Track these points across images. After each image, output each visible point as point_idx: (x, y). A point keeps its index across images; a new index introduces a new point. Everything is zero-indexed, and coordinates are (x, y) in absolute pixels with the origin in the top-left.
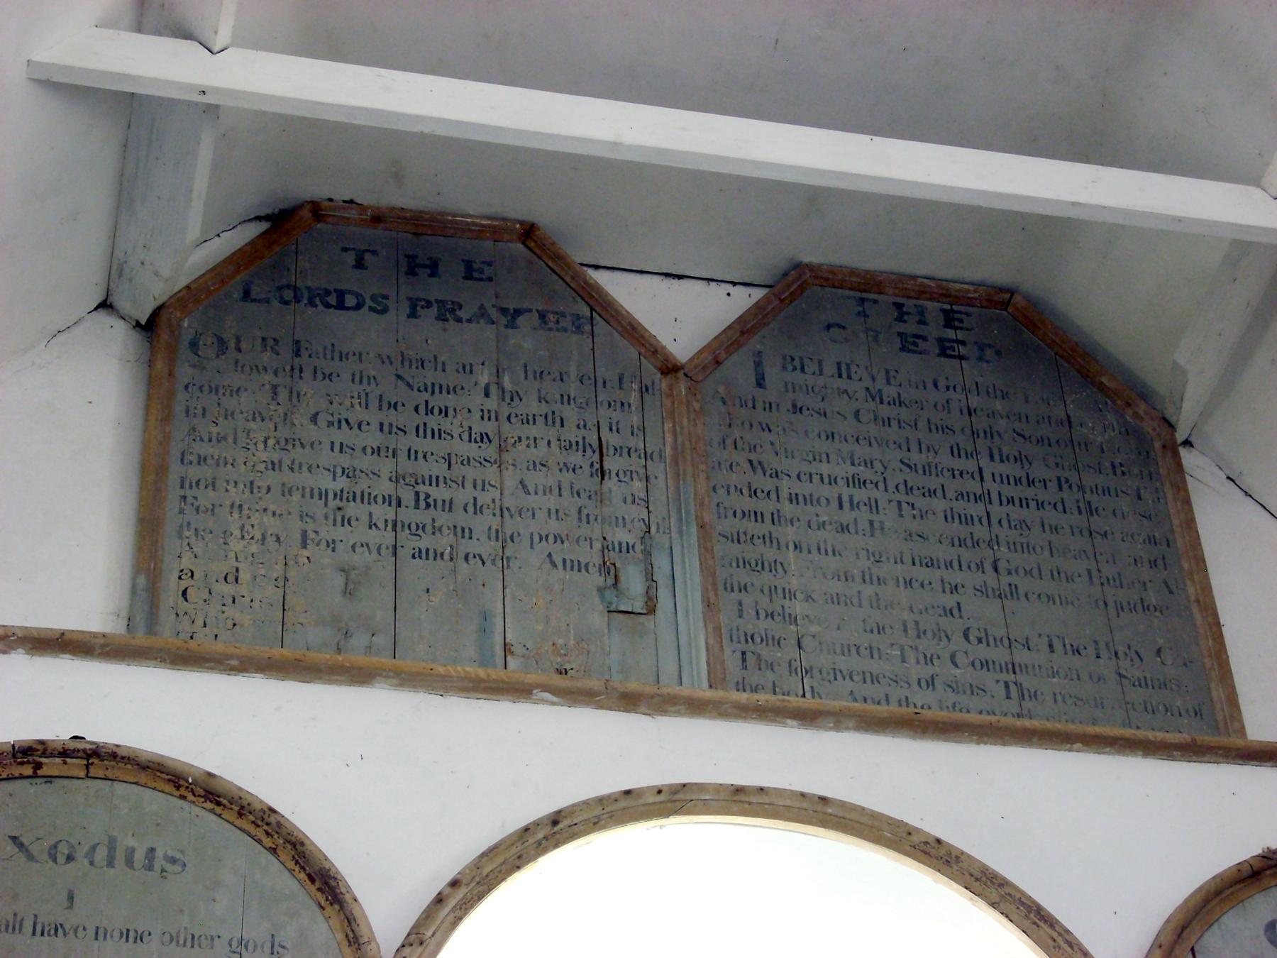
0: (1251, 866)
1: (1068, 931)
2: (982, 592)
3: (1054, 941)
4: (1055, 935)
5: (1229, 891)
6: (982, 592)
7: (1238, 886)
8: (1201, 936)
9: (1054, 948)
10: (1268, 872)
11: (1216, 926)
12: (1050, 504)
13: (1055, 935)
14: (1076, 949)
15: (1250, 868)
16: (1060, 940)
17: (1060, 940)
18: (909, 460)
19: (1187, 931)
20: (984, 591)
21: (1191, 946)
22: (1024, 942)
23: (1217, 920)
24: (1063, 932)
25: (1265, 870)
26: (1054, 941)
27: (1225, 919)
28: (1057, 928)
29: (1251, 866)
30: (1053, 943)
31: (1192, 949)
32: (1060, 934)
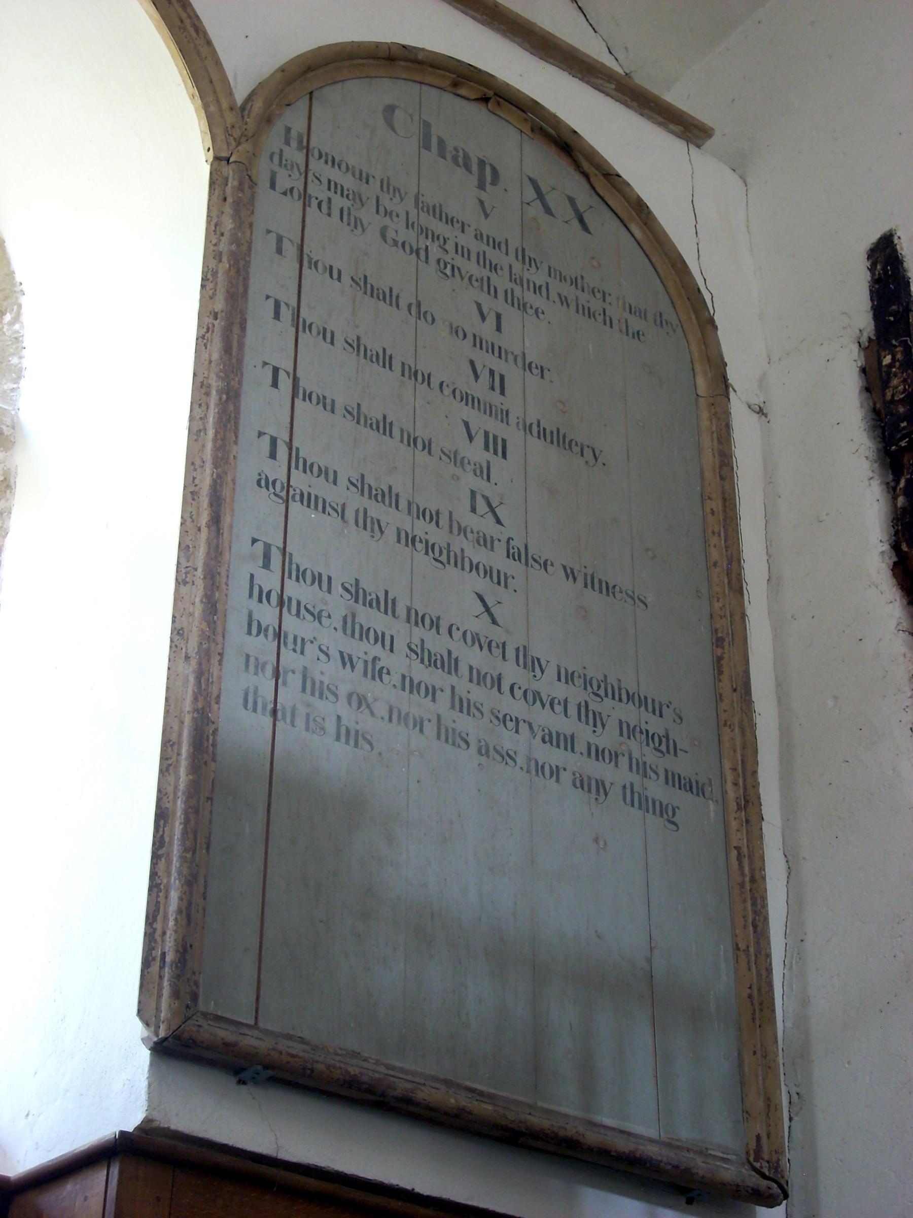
0: (389, 48)
1: (198, 17)
2: (417, 655)
3: (182, 22)
4: (184, 15)
5: (361, 61)
6: (417, 655)
7: (371, 61)
8: (323, 86)
9: (180, 28)
10: (403, 63)
11: (339, 86)
12: (520, 688)
13: (184, 15)
14: (201, 35)
15: (388, 50)
16: (187, 23)
17: (187, 23)
18: (320, 175)
19: (311, 74)
20: (355, 347)
21: (310, 90)
22: (151, 17)
23: (343, 81)
24: (193, 16)
25: (401, 60)
26: (182, 22)
27: (349, 84)
28: (189, 10)
29: (389, 48)
30: (180, 24)
31: (311, 93)
32: (189, 17)
